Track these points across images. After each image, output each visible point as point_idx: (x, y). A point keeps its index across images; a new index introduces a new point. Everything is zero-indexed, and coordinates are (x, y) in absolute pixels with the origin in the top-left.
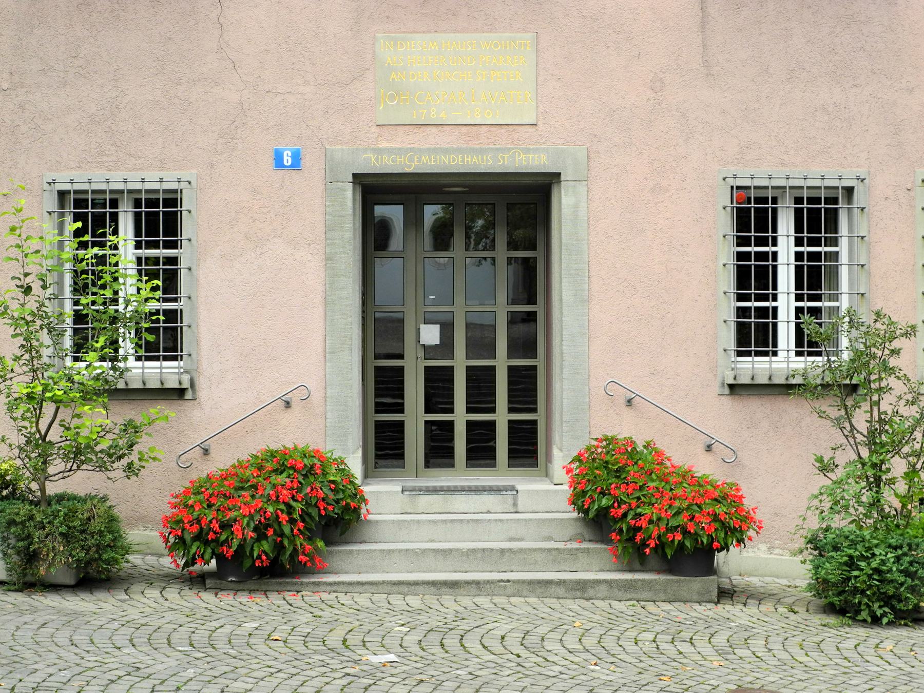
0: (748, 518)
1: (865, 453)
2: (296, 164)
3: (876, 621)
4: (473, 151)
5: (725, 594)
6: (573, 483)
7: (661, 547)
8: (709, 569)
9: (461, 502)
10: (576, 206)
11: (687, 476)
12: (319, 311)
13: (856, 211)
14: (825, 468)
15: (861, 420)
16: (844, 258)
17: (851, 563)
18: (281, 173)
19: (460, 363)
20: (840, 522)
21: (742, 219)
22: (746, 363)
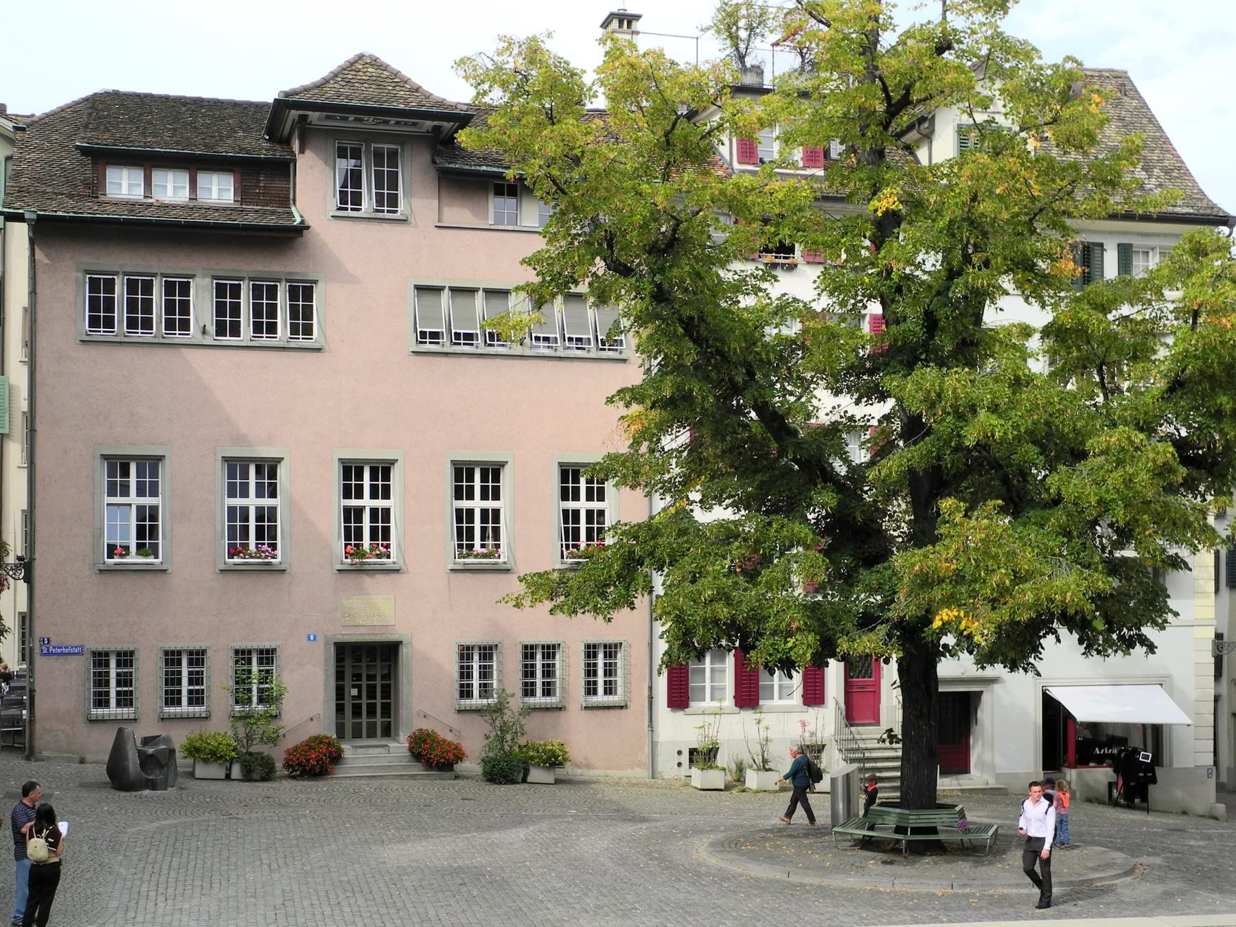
0: (463, 754)
1: (499, 733)
2: (315, 639)
3: (501, 783)
5: (457, 777)
6: (410, 743)
7: (437, 765)
8: (452, 770)
9: (371, 751)
11: (444, 741)
12: (322, 688)
14: (487, 737)
15: (497, 723)
16: (495, 667)
17: (494, 766)
19: (364, 701)
20: (491, 755)
21: (462, 657)
22: (463, 702)
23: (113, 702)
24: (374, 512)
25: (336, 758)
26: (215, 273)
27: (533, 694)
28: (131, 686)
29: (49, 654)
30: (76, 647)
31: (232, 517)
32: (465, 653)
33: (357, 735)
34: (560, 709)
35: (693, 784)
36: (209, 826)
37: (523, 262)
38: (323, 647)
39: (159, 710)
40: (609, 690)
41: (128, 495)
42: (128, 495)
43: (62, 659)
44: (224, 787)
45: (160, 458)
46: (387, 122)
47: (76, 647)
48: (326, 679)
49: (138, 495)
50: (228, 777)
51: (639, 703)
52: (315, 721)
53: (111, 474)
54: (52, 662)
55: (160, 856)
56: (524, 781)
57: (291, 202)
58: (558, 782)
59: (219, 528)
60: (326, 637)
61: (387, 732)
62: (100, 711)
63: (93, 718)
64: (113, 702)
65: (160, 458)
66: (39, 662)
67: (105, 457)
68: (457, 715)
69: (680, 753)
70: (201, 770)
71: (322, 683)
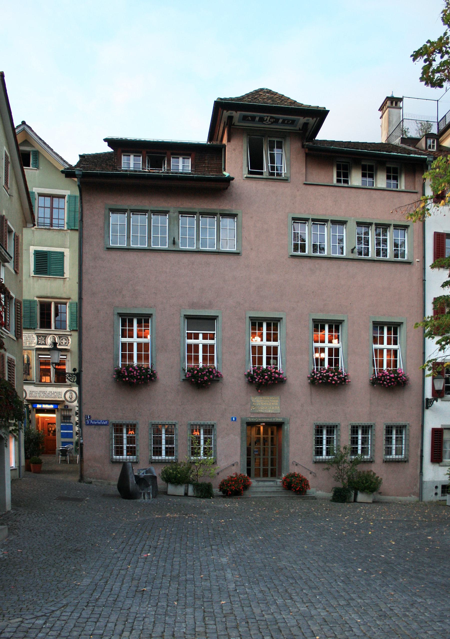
4: (268, 418)
5: (308, 498)
10: (287, 428)
12: (239, 448)
13: (407, 430)
18: (233, 422)
22: (318, 457)
23: (164, 452)
24: (205, 346)
25: (246, 487)
26: (180, 210)
27: (122, 454)
28: (134, 443)
29: (90, 424)
30: (105, 421)
31: (189, 350)
32: (319, 430)
33: (257, 475)
34: (405, 462)
35: (447, 504)
36: (174, 521)
37: (106, 140)
38: (240, 425)
39: (150, 458)
40: (170, 452)
41: (132, 337)
42: (132, 337)
43: (97, 427)
44: (190, 502)
45: (150, 315)
46: (276, 121)
47: (105, 421)
48: (242, 443)
49: (388, 344)
50: (186, 494)
51: (414, 459)
52: (235, 465)
53: (123, 325)
54: (92, 429)
55: (138, 540)
56: (355, 501)
57: (223, 170)
58: (374, 502)
59: (182, 355)
60: (241, 418)
61: (273, 474)
62: (157, 458)
63: (114, 461)
64: (164, 452)
65: (150, 315)
66: (85, 428)
67: (120, 315)
68: (314, 465)
69: (436, 487)
70: (171, 489)
71: (239, 445)
